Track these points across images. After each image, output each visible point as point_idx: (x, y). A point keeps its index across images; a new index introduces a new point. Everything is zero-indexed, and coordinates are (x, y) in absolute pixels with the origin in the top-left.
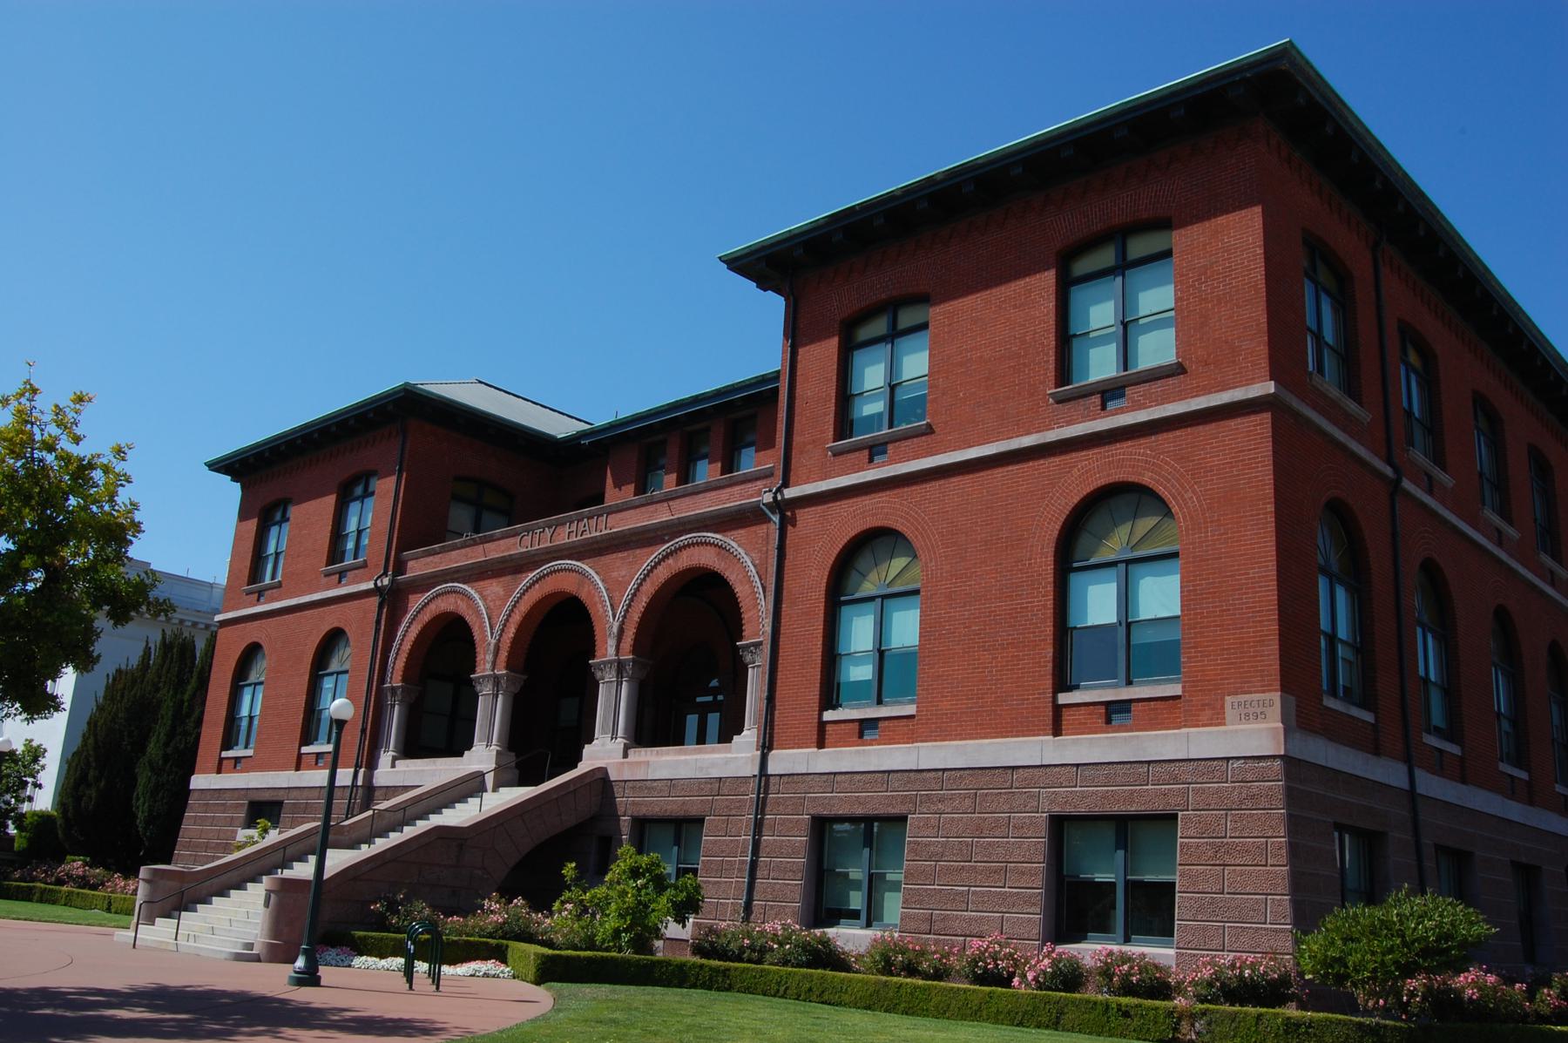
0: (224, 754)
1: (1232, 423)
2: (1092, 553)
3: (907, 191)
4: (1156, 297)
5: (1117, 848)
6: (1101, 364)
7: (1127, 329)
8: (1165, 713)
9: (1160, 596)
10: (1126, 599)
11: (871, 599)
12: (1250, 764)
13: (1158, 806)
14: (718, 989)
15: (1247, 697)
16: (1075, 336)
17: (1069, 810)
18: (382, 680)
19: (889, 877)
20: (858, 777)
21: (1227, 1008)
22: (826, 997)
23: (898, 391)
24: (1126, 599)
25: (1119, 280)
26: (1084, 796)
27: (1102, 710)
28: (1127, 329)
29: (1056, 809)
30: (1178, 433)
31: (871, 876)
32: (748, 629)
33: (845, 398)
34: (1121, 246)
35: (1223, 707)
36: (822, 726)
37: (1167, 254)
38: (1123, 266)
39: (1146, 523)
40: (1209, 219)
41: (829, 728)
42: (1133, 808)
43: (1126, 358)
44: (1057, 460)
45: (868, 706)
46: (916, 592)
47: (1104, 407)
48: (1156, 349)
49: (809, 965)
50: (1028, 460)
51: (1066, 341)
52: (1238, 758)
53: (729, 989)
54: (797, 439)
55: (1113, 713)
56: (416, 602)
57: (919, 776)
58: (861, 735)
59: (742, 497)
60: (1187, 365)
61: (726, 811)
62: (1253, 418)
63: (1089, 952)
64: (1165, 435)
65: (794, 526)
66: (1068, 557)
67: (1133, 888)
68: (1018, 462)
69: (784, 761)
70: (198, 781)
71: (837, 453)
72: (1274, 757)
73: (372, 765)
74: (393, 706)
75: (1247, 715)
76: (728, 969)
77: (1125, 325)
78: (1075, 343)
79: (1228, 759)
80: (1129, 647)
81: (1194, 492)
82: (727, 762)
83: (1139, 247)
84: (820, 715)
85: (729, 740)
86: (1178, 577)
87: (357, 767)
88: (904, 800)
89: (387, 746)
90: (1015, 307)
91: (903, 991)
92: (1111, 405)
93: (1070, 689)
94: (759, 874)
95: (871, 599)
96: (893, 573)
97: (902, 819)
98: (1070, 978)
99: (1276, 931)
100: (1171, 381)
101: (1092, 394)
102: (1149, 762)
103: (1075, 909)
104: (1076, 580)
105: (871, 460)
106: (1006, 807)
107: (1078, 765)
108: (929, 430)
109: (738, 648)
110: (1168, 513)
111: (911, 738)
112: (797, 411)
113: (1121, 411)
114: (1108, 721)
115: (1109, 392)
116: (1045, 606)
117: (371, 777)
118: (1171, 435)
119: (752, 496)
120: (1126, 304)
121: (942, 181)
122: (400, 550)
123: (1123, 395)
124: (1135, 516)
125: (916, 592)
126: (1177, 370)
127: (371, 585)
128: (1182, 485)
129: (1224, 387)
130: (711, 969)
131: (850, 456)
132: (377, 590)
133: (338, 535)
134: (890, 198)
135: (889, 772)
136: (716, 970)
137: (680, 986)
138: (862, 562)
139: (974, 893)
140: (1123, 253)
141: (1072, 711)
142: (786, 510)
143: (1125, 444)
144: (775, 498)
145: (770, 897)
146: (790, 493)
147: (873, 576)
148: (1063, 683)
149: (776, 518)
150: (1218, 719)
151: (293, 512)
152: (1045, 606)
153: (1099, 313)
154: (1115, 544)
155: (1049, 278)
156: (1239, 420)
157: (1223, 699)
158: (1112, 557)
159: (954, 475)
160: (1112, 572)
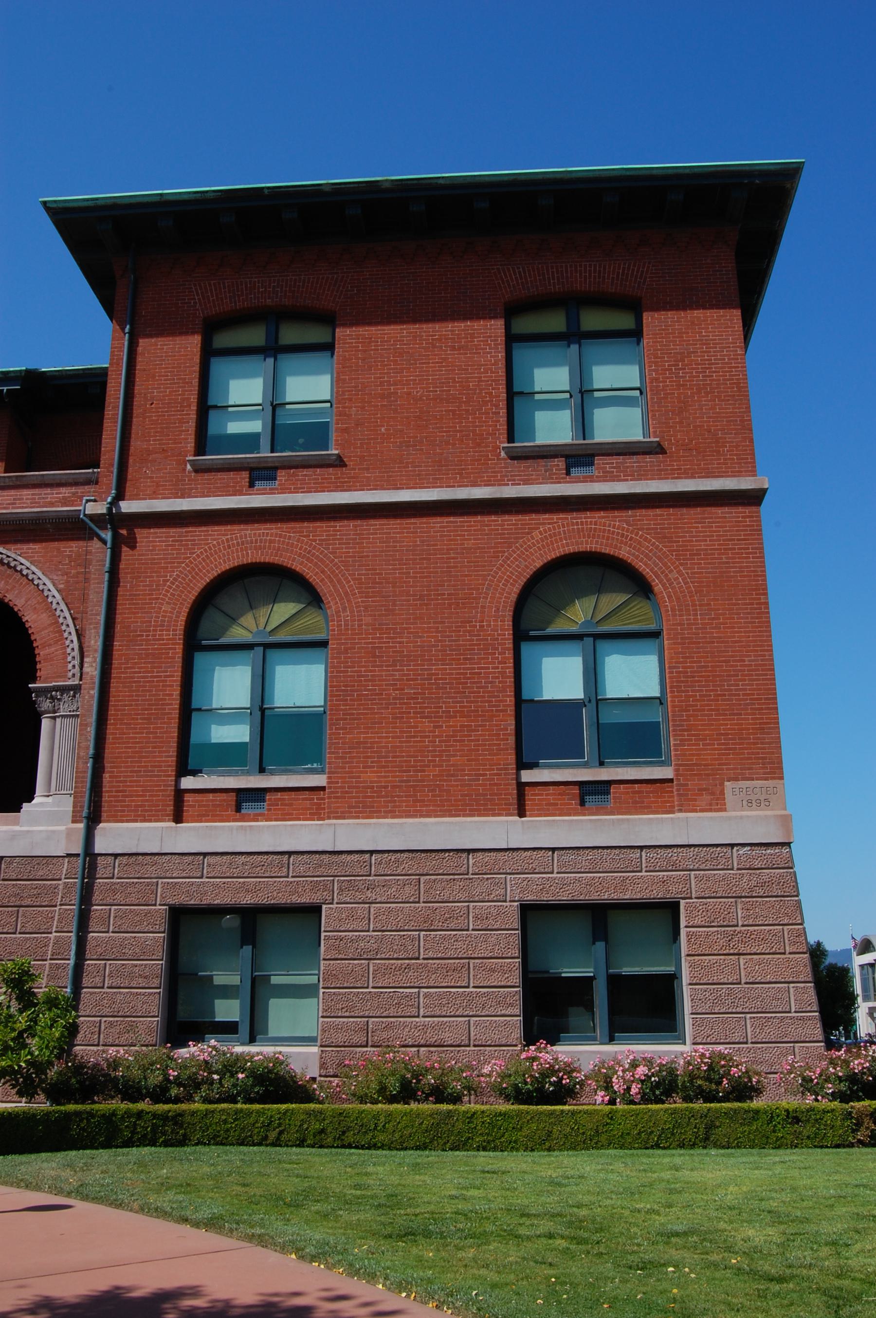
0: (527, 776)
1: (719, 511)
2: (549, 623)
3: (339, 190)
4: (614, 373)
5: (244, 943)
6: (553, 428)
7: (583, 399)
8: (652, 796)
10: (593, 675)
12: (757, 851)
13: (657, 893)
14: (166, 1144)
15: (748, 783)
17: (546, 897)
19: (274, 980)
20: (243, 858)
21: (644, 1106)
22: (350, 1137)
23: (279, 412)
24: (593, 675)
25: (270, 361)
26: (564, 884)
27: (576, 791)
29: (530, 897)
30: (658, 511)
31: (254, 980)
32: (44, 669)
33: (205, 408)
35: (722, 793)
36: (179, 794)
37: (329, 347)
38: (273, 350)
39: (612, 600)
40: (684, 309)
41: (187, 797)
42: (606, 896)
43: (583, 424)
44: (513, 519)
45: (248, 773)
48: (617, 425)
49: (263, 1099)
50: (475, 514)
51: (515, 396)
52: (743, 845)
53: (182, 1142)
54: (135, 444)
55: (590, 794)
57: (334, 858)
58: (238, 809)
59: (34, 503)
60: (666, 445)
61: (13, 901)
62: (741, 509)
63: (582, 1054)
64: (644, 512)
65: (133, 547)
67: (616, 982)
68: (462, 514)
69: (112, 837)
71: (199, 469)
75: (750, 802)
76: (181, 1114)
77: (582, 393)
79: (732, 846)
80: (280, 735)
81: (679, 572)
82: (14, 836)
84: (177, 782)
85: (18, 809)
88: (315, 886)
90: (453, 348)
91: (477, 1121)
92: (259, 485)
93: (194, 773)
94: (85, 982)
96: (274, 623)
97: (315, 910)
98: (555, 1090)
99: (802, 1019)
100: (648, 458)
101: (555, 456)
102: (641, 848)
103: (549, 1008)
105: (251, 485)
106: (462, 896)
107: (553, 850)
108: (339, 462)
109: (30, 691)
111: (317, 814)
112: (136, 411)
113: (585, 480)
114: (582, 803)
115: (578, 457)
116: (503, 673)
118: (651, 512)
119: (52, 504)
120: (275, 386)
121: (387, 190)
124: (600, 590)
127: (100, 508)
128: (665, 564)
129: (709, 474)
130: (155, 1115)
131: (220, 475)
134: (315, 191)
135: (290, 853)
136: (164, 1117)
137: (107, 1145)
140: (573, 321)
141: (537, 790)
142: (124, 528)
143: (597, 515)
144: (110, 509)
145: (106, 1011)
146: (127, 506)
147: (248, 620)
148: (184, 769)
149: (108, 536)
150: (717, 803)
152: (503, 673)
154: (579, 614)
155: (194, 342)
156: (726, 509)
157: (722, 784)
158: (574, 629)
159: (374, 517)
160: (249, 655)
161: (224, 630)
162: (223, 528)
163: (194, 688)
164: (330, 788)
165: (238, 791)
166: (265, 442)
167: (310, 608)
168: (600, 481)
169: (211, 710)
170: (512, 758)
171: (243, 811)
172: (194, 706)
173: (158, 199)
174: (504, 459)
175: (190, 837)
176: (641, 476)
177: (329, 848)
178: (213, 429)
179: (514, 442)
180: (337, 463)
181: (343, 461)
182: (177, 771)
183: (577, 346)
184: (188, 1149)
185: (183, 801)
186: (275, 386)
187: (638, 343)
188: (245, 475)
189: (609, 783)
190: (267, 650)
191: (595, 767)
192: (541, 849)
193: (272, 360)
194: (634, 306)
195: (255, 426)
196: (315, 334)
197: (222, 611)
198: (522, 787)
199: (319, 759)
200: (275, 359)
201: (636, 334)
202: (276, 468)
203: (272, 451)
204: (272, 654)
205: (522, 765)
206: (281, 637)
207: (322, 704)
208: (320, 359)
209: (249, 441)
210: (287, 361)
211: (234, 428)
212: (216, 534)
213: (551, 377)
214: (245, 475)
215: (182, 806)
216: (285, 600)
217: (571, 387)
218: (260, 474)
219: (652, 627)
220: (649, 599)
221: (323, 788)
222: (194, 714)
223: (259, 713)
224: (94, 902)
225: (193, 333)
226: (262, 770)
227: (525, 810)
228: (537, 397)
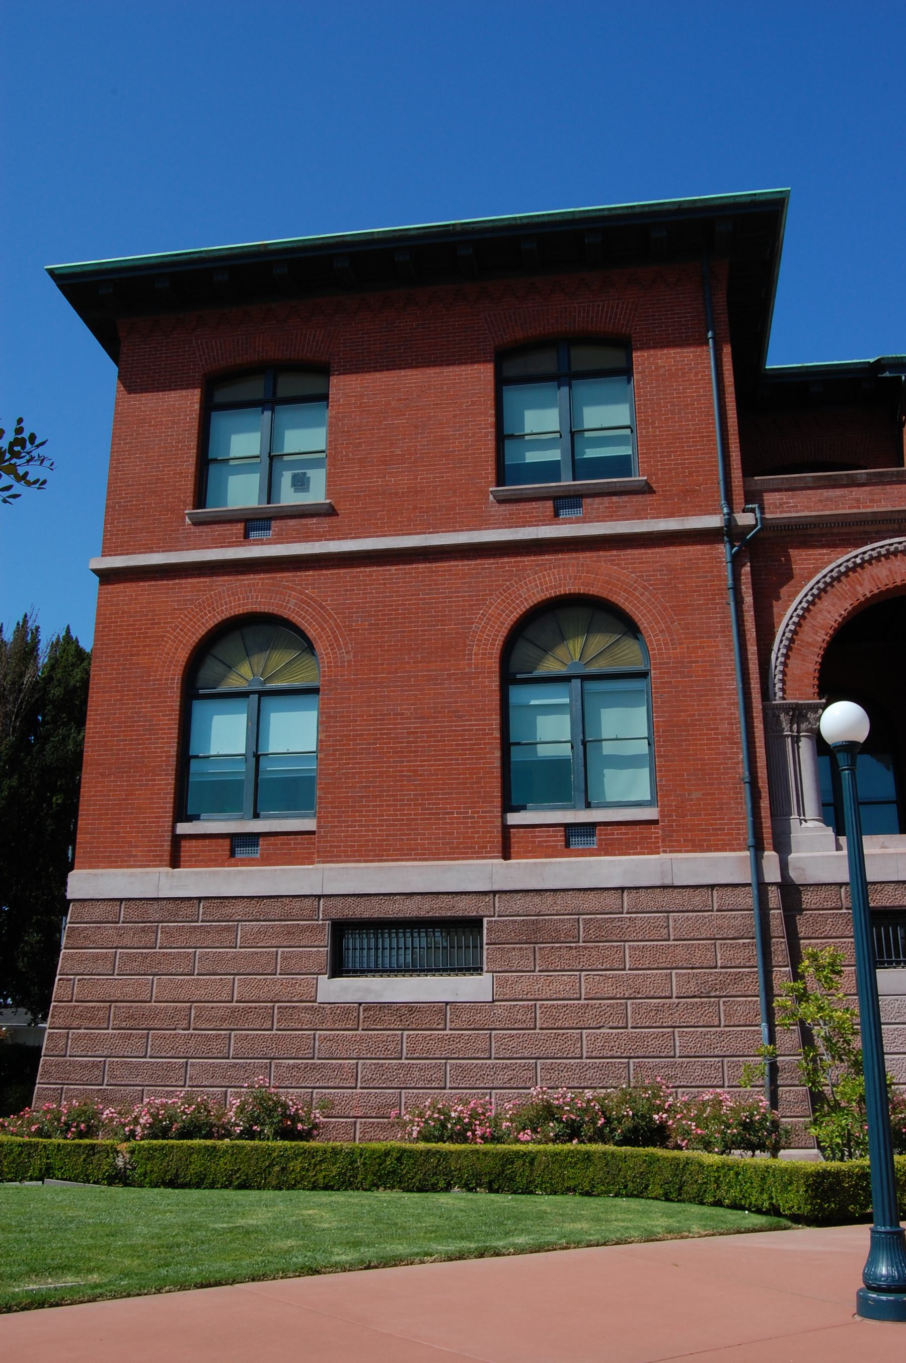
0: (183, 828)
4: (305, 437)
6: (242, 492)
9: (294, 732)
10: (257, 731)
11: (245, 694)
16: (215, 460)
18: (766, 694)
24: (257, 731)
25: (268, 414)
27: (227, 842)
28: (273, 460)
33: (502, 437)
34: (583, 356)
36: (506, 829)
37: (324, 398)
39: (599, 642)
43: (270, 489)
45: (573, 808)
46: (315, 691)
47: (246, 536)
51: (206, 463)
56: (814, 568)
58: (232, 854)
66: (514, 668)
70: (81, 883)
71: (198, 523)
72: (841, 885)
73: (783, 846)
74: (796, 740)
78: (213, 470)
80: (262, 784)
83: (287, 385)
84: (174, 828)
86: (315, 713)
87: (758, 848)
89: (801, 810)
92: (564, 514)
95: (245, 694)
104: (199, 708)
108: (647, 489)
110: (309, 647)
113: (261, 543)
115: (252, 523)
117: (784, 866)
120: (273, 438)
122: (749, 471)
123: (580, 506)
124: (589, 630)
125: (315, 691)
126: (330, 512)
127: (714, 521)
132: (730, 532)
133: (502, 437)
134: (680, 210)
138: (227, 648)
139: (193, 1065)
147: (245, 670)
148: (181, 814)
151: (341, 386)
153: (243, 441)
154: (244, 675)
155: (195, 396)
160: (242, 703)
161: (222, 678)
162: (595, 554)
163: (191, 739)
164: (663, 821)
165: (567, 826)
166: (566, 470)
167: (303, 654)
168: (270, 544)
169: (208, 757)
170: (498, 802)
171: (238, 856)
172: (191, 753)
173: (749, 199)
174: (492, 503)
175: (520, 873)
176: (638, 515)
177: (658, 883)
178: (510, 460)
179: (204, 508)
180: (330, 511)
181: (651, 488)
182: (173, 817)
183: (270, 413)
184: (296, 1192)
185: (180, 847)
186: (572, 416)
187: (629, 381)
188: (550, 504)
189: (594, 825)
190: (261, 698)
191: (581, 809)
192: (98, 900)
193: (270, 413)
194: (324, 371)
195: (554, 455)
196: (609, 357)
197: (536, 645)
198: (177, 840)
199: (310, 806)
200: (273, 412)
201: (626, 372)
202: (270, 519)
203: (574, 480)
204: (267, 702)
205: (508, 807)
206: (593, 669)
207: (569, 738)
208: (614, 385)
209: (550, 470)
210: (285, 414)
211: (532, 457)
212: (222, 582)
213: (243, 441)
214: (550, 504)
215: (179, 852)
216: (599, 631)
217: (632, 421)
218: (565, 502)
219: (641, 668)
220: (637, 638)
221: (655, 822)
222: (512, 748)
223: (254, 759)
224: (773, 934)
225: (485, 362)
226: (256, 816)
227: (179, 861)
228: (587, 434)
